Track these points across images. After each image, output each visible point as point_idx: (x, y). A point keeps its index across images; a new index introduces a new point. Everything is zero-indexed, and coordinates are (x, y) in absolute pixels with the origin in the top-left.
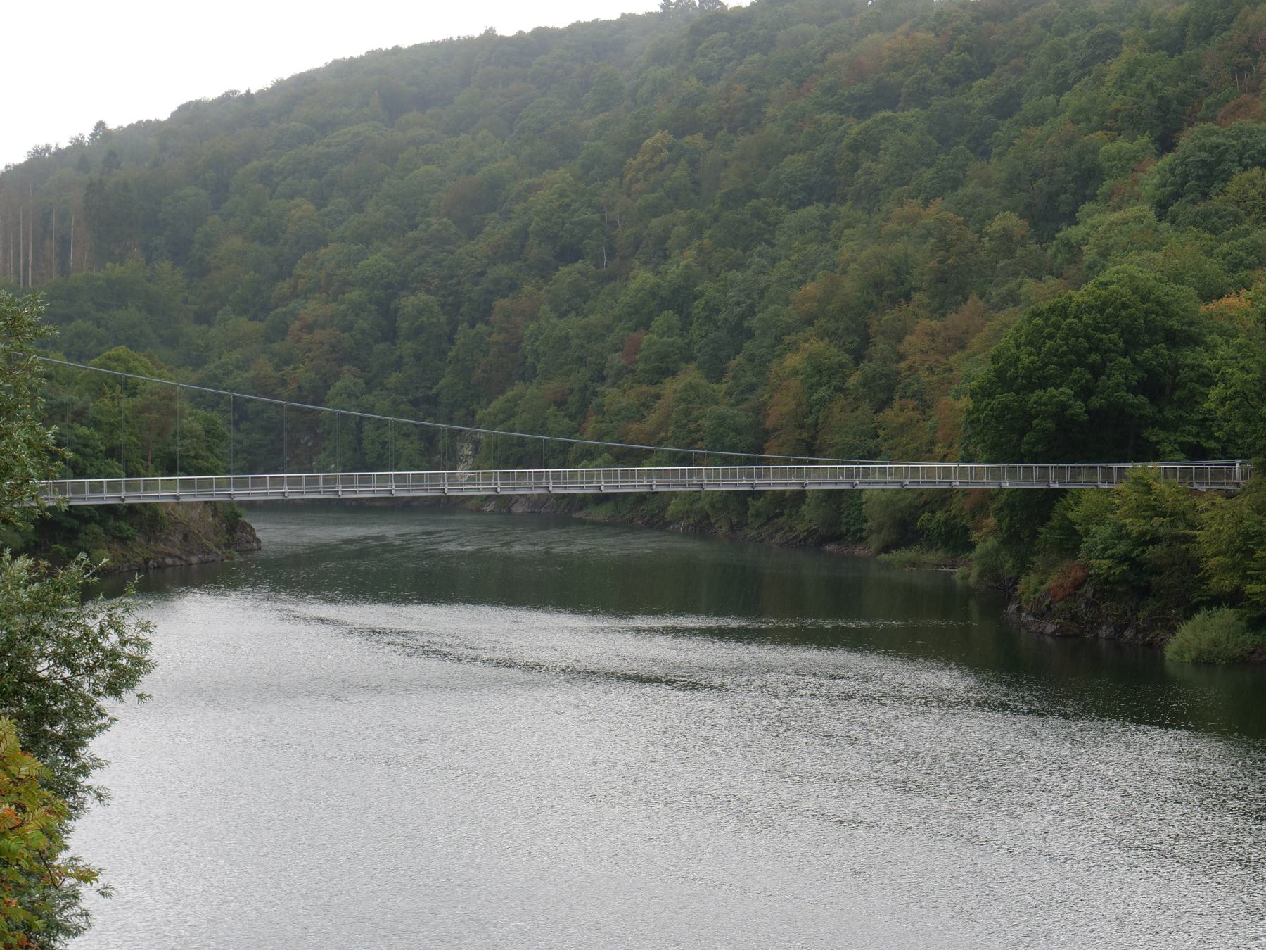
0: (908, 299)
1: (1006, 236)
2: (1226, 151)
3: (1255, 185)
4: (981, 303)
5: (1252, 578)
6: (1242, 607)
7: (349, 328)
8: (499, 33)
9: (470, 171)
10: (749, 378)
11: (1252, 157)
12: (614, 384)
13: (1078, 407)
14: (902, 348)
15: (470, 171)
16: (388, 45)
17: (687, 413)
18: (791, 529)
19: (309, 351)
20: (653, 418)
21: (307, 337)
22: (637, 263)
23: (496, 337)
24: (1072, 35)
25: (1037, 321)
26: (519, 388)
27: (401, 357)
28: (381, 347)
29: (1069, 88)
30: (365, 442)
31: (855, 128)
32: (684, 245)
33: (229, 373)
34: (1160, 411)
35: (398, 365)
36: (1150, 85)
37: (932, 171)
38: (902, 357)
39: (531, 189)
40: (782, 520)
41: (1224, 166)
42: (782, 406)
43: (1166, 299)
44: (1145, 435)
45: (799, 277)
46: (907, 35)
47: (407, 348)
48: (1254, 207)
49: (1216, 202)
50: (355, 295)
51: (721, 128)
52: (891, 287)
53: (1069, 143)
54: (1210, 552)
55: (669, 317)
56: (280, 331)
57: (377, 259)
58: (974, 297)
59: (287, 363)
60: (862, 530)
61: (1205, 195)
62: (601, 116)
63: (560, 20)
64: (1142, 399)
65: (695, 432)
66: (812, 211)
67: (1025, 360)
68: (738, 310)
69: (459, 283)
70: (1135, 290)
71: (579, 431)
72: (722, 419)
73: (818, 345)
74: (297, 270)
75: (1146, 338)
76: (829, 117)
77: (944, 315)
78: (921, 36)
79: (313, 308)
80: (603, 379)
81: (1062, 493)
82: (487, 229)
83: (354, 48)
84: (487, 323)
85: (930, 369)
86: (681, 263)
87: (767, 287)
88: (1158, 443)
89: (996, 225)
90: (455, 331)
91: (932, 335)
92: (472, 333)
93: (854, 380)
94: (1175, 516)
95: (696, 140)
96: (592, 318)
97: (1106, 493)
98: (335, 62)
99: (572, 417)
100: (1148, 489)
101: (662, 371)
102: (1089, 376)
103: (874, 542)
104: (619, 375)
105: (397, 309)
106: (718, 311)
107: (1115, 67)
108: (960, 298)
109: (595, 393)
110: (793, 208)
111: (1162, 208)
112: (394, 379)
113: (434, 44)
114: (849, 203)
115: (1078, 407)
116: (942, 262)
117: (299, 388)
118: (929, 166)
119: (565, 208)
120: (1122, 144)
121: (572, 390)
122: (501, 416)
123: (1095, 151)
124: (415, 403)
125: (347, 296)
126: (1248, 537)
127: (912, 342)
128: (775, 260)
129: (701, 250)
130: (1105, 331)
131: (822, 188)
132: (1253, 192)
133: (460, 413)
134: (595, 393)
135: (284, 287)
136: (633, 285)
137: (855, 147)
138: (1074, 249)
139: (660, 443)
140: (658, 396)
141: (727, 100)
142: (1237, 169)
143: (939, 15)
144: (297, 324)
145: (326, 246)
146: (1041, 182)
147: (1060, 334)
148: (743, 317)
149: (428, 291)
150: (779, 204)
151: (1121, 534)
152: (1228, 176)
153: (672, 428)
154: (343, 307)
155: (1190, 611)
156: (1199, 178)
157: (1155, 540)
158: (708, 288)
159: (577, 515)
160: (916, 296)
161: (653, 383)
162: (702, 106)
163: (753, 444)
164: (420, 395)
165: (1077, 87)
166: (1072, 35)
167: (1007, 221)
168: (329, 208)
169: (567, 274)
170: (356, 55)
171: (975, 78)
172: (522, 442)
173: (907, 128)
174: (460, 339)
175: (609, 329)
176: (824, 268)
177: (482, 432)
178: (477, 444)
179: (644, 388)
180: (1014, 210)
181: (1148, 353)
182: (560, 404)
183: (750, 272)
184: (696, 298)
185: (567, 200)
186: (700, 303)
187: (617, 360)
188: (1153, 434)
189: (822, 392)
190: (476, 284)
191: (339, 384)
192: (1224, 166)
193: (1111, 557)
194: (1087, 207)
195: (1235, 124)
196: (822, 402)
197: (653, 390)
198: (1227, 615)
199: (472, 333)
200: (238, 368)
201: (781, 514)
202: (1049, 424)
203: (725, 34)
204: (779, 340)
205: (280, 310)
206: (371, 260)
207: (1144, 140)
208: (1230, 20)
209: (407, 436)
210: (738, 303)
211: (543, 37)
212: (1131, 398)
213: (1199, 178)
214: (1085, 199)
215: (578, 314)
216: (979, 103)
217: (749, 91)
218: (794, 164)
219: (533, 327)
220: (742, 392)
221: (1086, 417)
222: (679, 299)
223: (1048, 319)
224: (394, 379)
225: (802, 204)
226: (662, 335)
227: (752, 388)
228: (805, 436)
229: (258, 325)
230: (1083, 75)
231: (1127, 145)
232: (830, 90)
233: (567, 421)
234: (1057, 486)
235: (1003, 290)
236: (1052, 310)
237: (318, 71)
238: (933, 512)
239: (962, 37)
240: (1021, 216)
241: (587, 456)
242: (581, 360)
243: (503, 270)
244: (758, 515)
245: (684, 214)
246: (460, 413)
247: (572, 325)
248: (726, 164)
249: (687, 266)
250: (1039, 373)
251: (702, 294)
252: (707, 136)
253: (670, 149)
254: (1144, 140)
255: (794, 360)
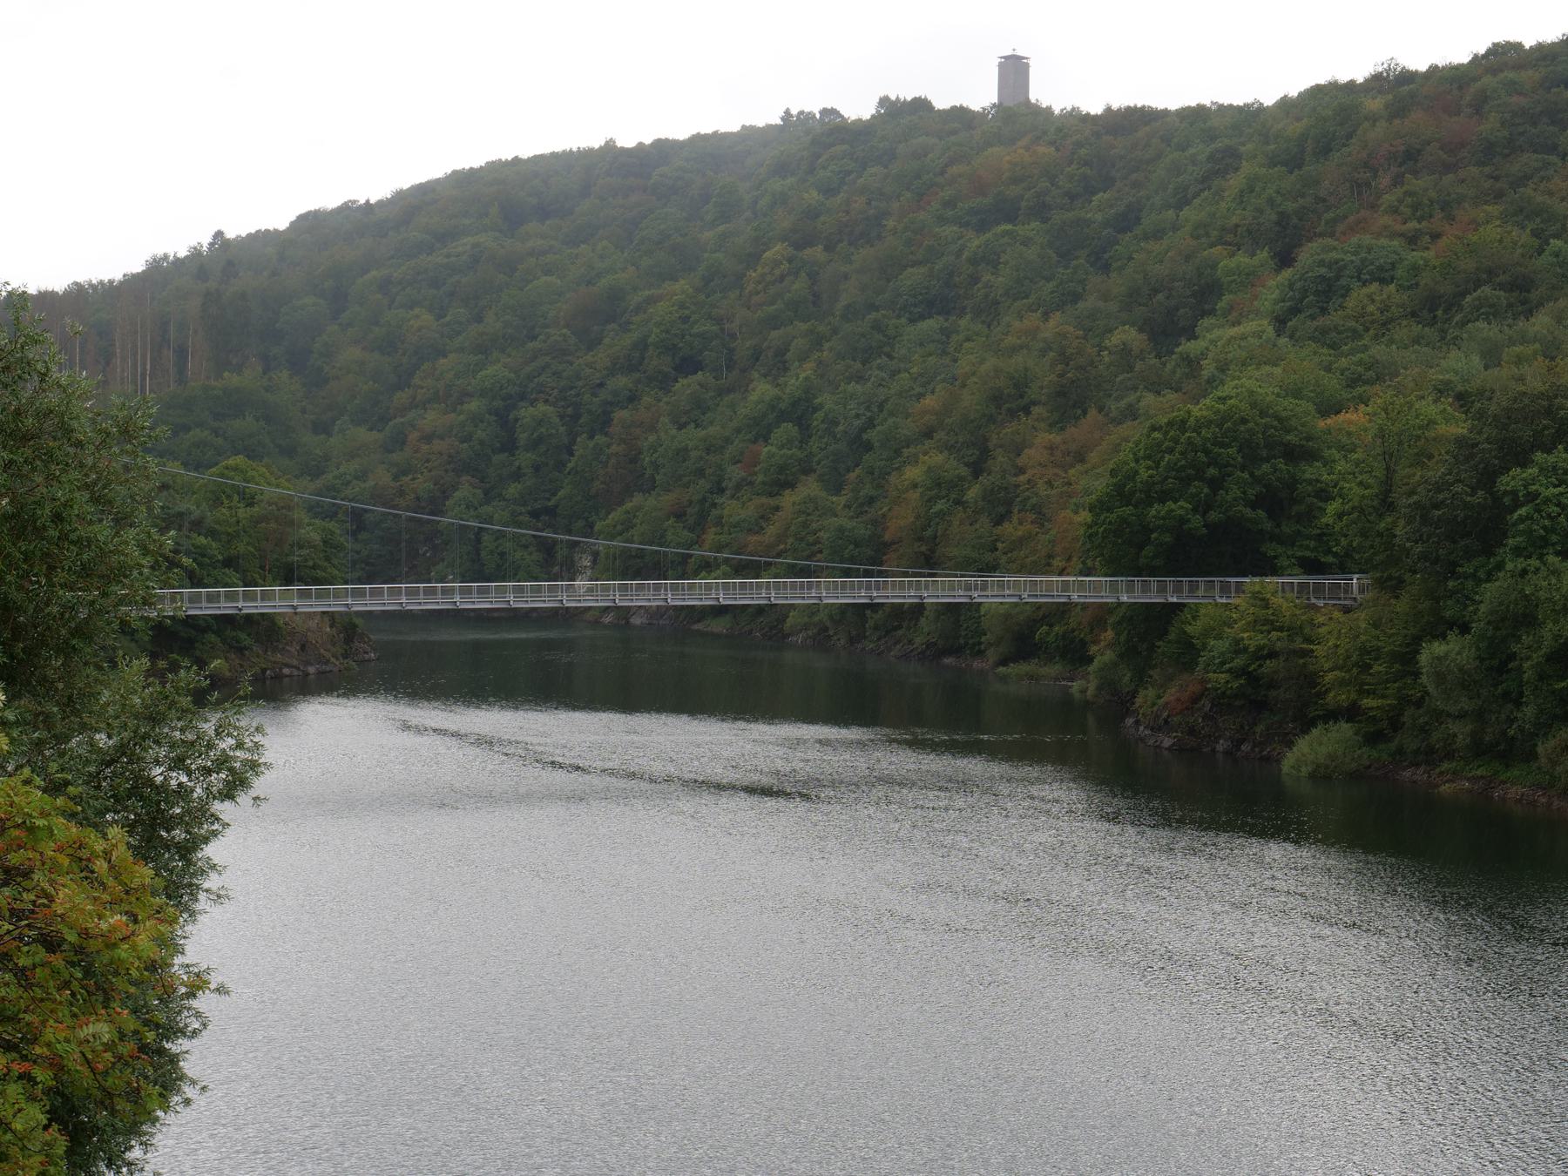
0: (1026, 410)
1: (1125, 350)
2: (1345, 267)
3: (1373, 301)
4: (1100, 417)
5: (1369, 692)
6: (1359, 722)
7: (467, 439)
8: (619, 144)
9: (589, 283)
10: (867, 490)
11: (1371, 273)
12: (733, 497)
13: (1196, 521)
14: (1020, 461)
15: (589, 283)
16: (507, 155)
17: (805, 525)
18: (910, 642)
19: (428, 461)
20: (772, 531)
21: (425, 447)
22: (756, 375)
23: (614, 448)
24: (1192, 151)
25: (1156, 435)
26: (638, 499)
27: (519, 468)
28: (498, 458)
29: (1188, 202)
30: (483, 554)
31: (975, 242)
32: (803, 359)
33: (349, 482)
34: (1278, 526)
35: (517, 476)
36: (1271, 202)
37: (1051, 285)
38: (1022, 471)
39: (651, 301)
40: (900, 632)
41: (1343, 282)
42: (901, 519)
43: (1284, 414)
44: (1263, 549)
45: (919, 390)
46: (1027, 149)
47: (525, 459)
48: (1372, 322)
49: (1334, 318)
50: (474, 405)
51: (840, 241)
52: (1010, 400)
53: (1188, 258)
54: (1327, 666)
55: (788, 429)
56: (399, 441)
57: (497, 370)
58: (1092, 412)
59: (405, 473)
60: (980, 643)
61: (1324, 311)
62: (721, 228)
63: (681, 133)
64: (1261, 513)
65: (814, 544)
66: (931, 325)
67: (1144, 474)
68: (857, 423)
69: (578, 395)
70: (1253, 405)
71: (698, 542)
72: (841, 530)
73: (938, 458)
74: (416, 381)
75: (1264, 453)
76: (949, 231)
77: (1062, 429)
78: (1041, 149)
79: (432, 418)
80: (722, 491)
81: (1179, 607)
82: (606, 341)
83: (474, 157)
84: (606, 434)
85: (1050, 484)
86: (799, 377)
87: (887, 400)
88: (1275, 557)
89: (1115, 339)
90: (573, 442)
91: (1051, 448)
92: (591, 444)
93: (973, 493)
94: (1293, 630)
95: (817, 253)
96: (711, 430)
97: (1222, 606)
98: (455, 172)
99: (691, 530)
100: (1266, 604)
101: (782, 482)
102: (1206, 490)
103: (992, 655)
104: (738, 487)
105: (517, 420)
106: (837, 424)
107: (1235, 182)
108: (1079, 412)
109: (714, 505)
110: (912, 321)
111: (1280, 322)
112: (513, 490)
113: (554, 155)
114: (968, 317)
115: (1196, 521)
116: (1061, 376)
117: (418, 498)
118: (1048, 280)
119: (685, 319)
120: (1242, 259)
121: (691, 502)
122: (619, 527)
123: (1214, 266)
124: (535, 514)
125: (466, 407)
126: (1364, 651)
127: (1032, 455)
128: (894, 373)
129: (820, 363)
130: (1222, 445)
131: (938, 303)
132: (1371, 308)
133: (581, 523)
134: (714, 505)
135: (402, 397)
136: (753, 397)
137: (973, 261)
138: (1192, 364)
139: (779, 555)
140: (777, 509)
141: (848, 212)
142: (1355, 284)
143: (1059, 130)
144: (416, 435)
145: (445, 356)
146: (1160, 296)
147: (1179, 448)
148: (863, 430)
149: (546, 401)
150: (899, 317)
151: (1238, 648)
152: (1347, 291)
153: (790, 541)
154: (462, 417)
155: (1306, 725)
156: (1317, 293)
157: (1272, 655)
158: (827, 400)
159: (696, 627)
160: (1036, 410)
161: (771, 495)
162: (822, 218)
163: (869, 556)
164: (538, 506)
165: (1197, 201)
166: (1192, 151)
167: (1127, 335)
168: (448, 318)
169: (686, 386)
170: (476, 165)
171: (1093, 193)
172: (640, 554)
173: (1026, 242)
174: (579, 450)
175: (728, 441)
176: (944, 381)
177: (601, 544)
178: (596, 555)
179: (764, 500)
180: (1133, 325)
181: (1266, 467)
182: (680, 516)
183: (869, 384)
184: (815, 410)
185: (687, 312)
186: (820, 415)
187: (735, 473)
188: (1270, 549)
189: (940, 506)
190: (594, 395)
191: (457, 494)
192: (1343, 282)
193: (1229, 671)
194: (1206, 322)
195: (1355, 240)
196: (941, 514)
197: (772, 502)
198: (1345, 729)
199: (591, 444)
200: (357, 478)
201: (900, 627)
202: (1167, 538)
203: (845, 147)
204: (898, 452)
205: (399, 420)
206: (490, 370)
207: (1263, 255)
208: (1349, 136)
209: (526, 547)
210: (857, 416)
211: (663, 148)
212: (1248, 512)
213: (1317, 293)
214: (1204, 314)
215: (697, 426)
216: (1099, 217)
217: (869, 204)
218: (912, 277)
219: (652, 438)
220: (862, 505)
221: (1204, 531)
222: (799, 412)
223: (1166, 433)
224: (513, 490)
225: (922, 317)
226: (782, 447)
227: (871, 500)
228: (923, 548)
229: (375, 435)
230: (1202, 190)
231: (1247, 260)
232: (950, 203)
233: (685, 532)
234: (1175, 600)
235: (1123, 404)
236: (1170, 424)
237: (438, 181)
238: (1051, 626)
239: (1083, 151)
240: (1141, 330)
241: (706, 567)
242: (700, 473)
243: (622, 382)
244: (876, 628)
245: (803, 327)
246: (581, 523)
247: (692, 436)
248: (846, 277)
249: (806, 379)
250: (1158, 487)
251: (821, 406)
252: (828, 249)
253: (790, 261)
254: (1263, 255)
255: (913, 473)
